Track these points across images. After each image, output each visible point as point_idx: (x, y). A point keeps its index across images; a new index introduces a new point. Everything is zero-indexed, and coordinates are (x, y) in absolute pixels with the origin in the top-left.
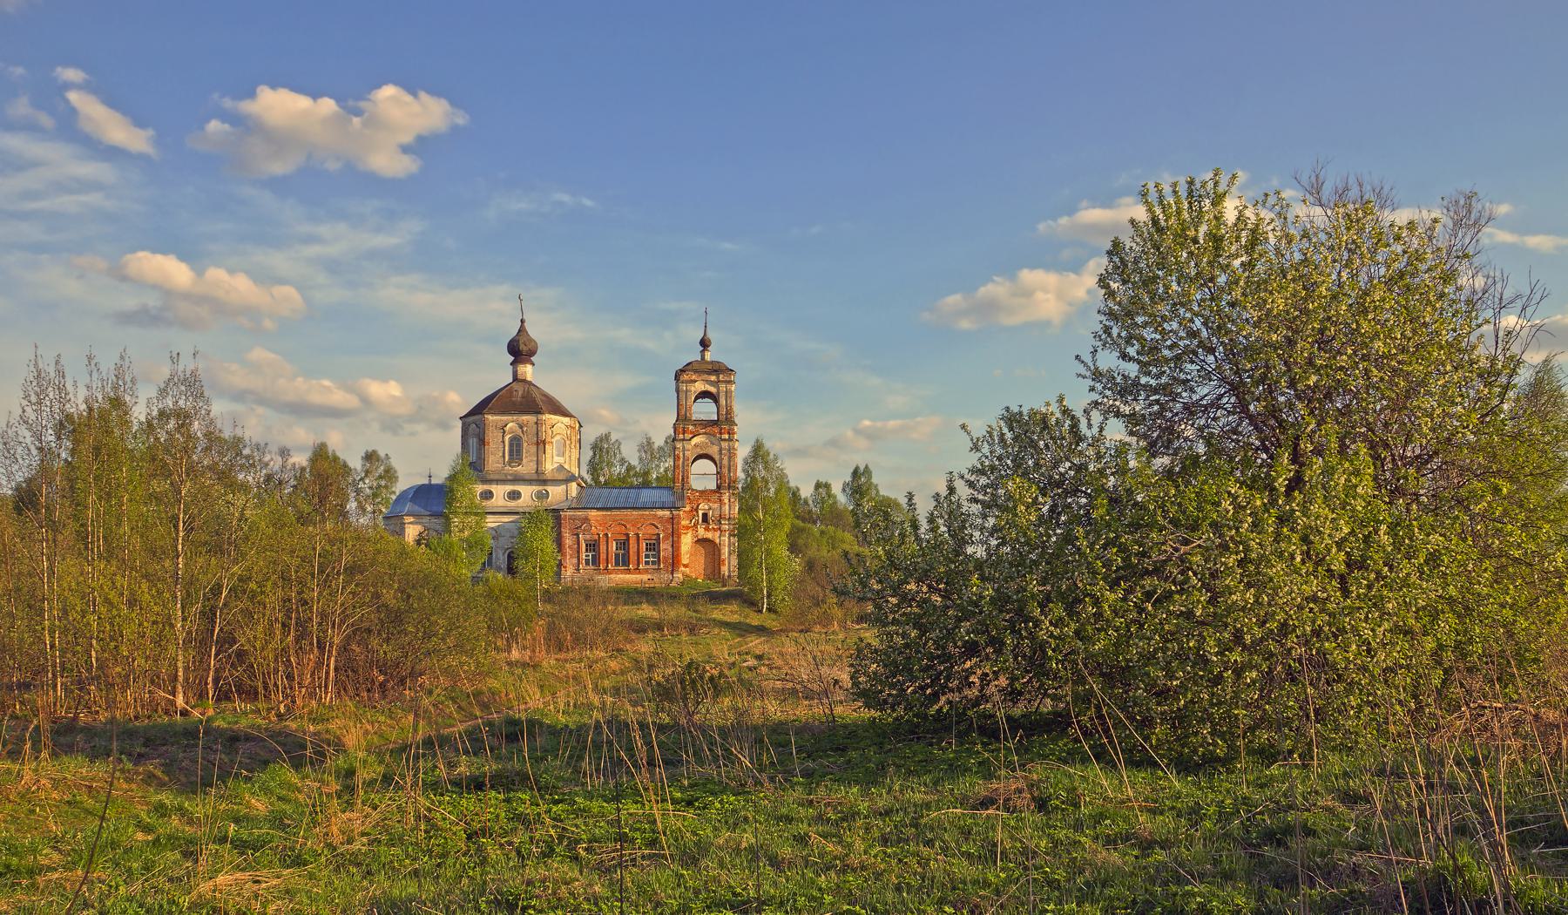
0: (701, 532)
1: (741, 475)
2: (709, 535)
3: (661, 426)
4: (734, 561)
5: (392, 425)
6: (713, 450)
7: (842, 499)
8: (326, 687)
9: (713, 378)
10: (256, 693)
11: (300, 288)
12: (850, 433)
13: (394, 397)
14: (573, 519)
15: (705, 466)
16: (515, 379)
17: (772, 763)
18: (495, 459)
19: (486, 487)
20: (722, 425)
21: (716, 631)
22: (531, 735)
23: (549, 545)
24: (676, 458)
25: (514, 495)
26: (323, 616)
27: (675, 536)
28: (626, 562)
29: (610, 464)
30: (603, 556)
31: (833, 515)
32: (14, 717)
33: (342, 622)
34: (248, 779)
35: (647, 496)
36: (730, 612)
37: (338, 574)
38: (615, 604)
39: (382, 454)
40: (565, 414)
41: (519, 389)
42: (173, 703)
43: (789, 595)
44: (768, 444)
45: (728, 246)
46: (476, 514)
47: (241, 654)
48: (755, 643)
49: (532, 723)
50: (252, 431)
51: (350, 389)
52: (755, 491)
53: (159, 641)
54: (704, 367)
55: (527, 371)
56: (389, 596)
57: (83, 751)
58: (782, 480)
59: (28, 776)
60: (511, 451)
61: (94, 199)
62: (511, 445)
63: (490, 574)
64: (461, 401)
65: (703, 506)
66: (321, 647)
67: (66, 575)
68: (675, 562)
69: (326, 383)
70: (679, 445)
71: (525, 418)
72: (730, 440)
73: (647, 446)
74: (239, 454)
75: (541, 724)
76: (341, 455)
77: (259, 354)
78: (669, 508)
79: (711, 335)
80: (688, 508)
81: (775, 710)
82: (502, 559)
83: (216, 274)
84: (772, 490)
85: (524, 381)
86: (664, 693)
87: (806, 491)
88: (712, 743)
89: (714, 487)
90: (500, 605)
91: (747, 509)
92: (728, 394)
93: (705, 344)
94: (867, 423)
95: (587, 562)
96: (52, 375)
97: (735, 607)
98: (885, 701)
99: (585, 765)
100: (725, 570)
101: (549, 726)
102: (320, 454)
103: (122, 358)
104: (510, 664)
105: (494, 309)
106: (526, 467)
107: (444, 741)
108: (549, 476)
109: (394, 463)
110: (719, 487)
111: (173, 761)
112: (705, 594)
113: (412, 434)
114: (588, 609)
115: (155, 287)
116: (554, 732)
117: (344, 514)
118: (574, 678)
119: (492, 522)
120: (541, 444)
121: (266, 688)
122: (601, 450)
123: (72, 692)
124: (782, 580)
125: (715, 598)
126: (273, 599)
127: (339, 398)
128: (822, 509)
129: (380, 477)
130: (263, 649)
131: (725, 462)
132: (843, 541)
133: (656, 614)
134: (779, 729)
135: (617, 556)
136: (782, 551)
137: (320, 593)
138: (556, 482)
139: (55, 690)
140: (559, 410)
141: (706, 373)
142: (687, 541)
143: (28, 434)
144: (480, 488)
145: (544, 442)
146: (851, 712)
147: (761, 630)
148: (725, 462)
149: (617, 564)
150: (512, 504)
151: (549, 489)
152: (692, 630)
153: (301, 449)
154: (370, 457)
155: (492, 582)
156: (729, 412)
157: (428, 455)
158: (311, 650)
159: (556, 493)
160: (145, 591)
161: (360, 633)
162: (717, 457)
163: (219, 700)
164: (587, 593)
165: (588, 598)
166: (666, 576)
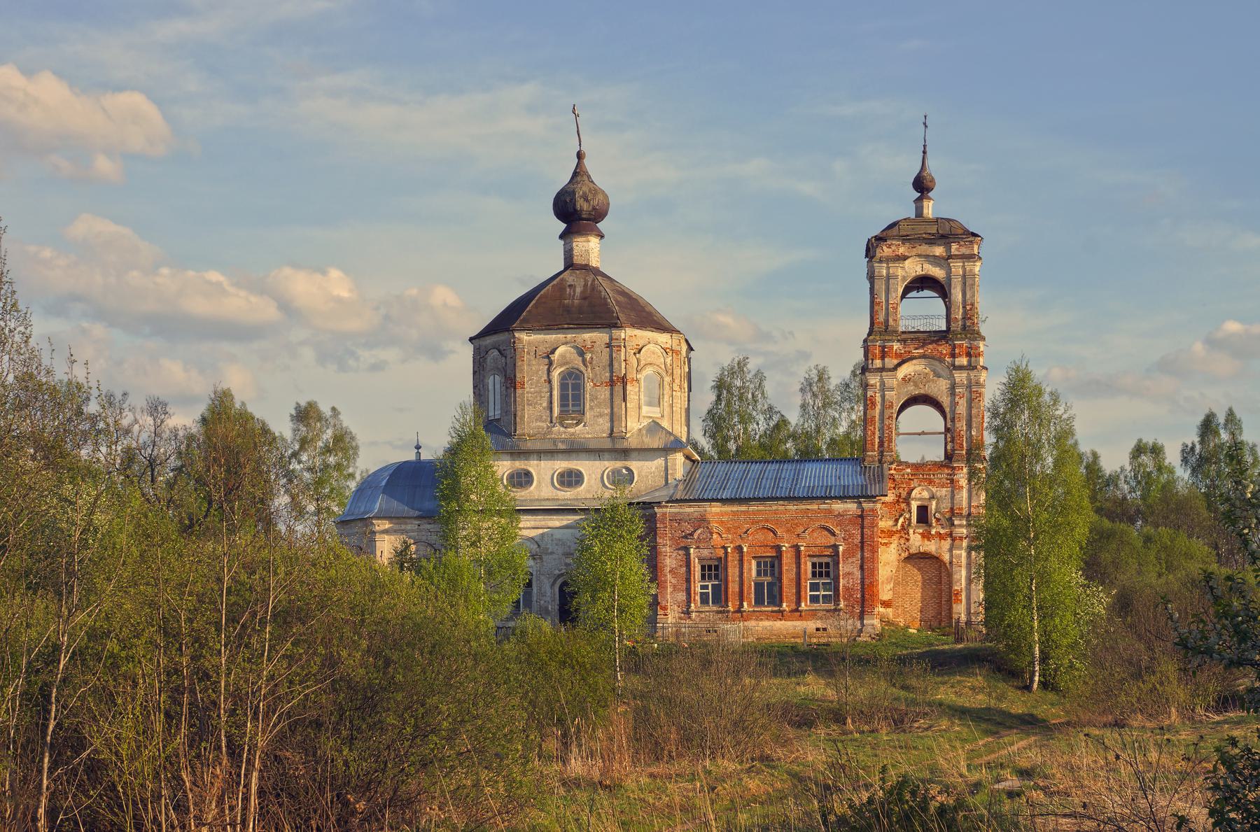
0: (916, 541)
2: (931, 547)
6: (939, 388)
9: (939, 251)
16: (569, 264)
18: (533, 416)
19: (519, 465)
25: (571, 479)
28: (776, 599)
30: (733, 587)
40: (661, 326)
54: (921, 230)
55: (590, 248)
60: (564, 398)
62: (563, 387)
65: (920, 494)
68: (865, 599)
70: (874, 380)
71: (587, 336)
72: (971, 367)
79: (933, 168)
85: (586, 268)
93: (922, 186)
95: (704, 599)
106: (593, 428)
110: (949, 457)
120: (618, 383)
135: (759, 586)
138: (645, 453)
140: (649, 319)
145: (624, 380)
148: (962, 409)
149: (759, 601)
150: (567, 495)
159: (646, 472)
166: (851, 624)
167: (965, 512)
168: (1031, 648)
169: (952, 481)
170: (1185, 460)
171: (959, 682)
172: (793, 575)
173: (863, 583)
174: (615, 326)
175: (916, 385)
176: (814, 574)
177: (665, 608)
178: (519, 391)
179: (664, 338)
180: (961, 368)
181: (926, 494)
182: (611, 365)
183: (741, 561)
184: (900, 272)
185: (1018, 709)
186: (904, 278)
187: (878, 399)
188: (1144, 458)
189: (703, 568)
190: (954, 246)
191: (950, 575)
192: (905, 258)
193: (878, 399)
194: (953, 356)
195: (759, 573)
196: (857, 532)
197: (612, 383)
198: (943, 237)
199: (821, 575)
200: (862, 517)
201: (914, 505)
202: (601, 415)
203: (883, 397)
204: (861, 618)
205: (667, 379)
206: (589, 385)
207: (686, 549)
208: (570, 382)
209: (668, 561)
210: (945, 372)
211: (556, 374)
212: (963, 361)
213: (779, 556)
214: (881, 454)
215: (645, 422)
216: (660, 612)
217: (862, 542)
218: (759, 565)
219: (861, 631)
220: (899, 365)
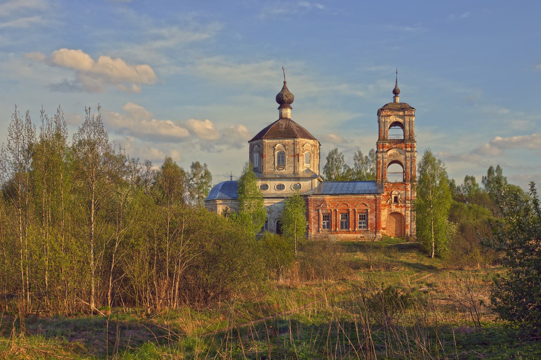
0: (394, 208)
1: (418, 175)
2: (398, 210)
3: (368, 143)
4: (414, 226)
5: (207, 146)
6: (401, 158)
7: (482, 186)
8: (174, 298)
9: (401, 113)
10: (135, 302)
11: (152, 67)
12: (487, 145)
13: (208, 130)
14: (315, 200)
15: (397, 168)
16: (281, 117)
17: (441, 351)
18: (269, 167)
19: (264, 182)
20: (407, 142)
21: (403, 269)
22: (294, 330)
23: (302, 217)
24: (378, 163)
25: (281, 187)
26: (172, 258)
27: (377, 211)
28: (347, 227)
29: (338, 168)
30: (333, 223)
31: (477, 198)
32: (6, 313)
33: (183, 262)
34: (132, 351)
35: (360, 186)
36: (412, 257)
37: (180, 234)
38: (341, 252)
39: (202, 164)
40: (311, 138)
41: (283, 123)
42: (89, 307)
43: (448, 247)
44: (434, 153)
45: (408, 29)
46: (257, 198)
47: (126, 280)
48: (428, 277)
49: (294, 323)
50: (129, 152)
51: (183, 126)
52: (426, 183)
53: (81, 271)
54: (396, 106)
55: (288, 112)
56: (209, 247)
57: (42, 333)
58: (443, 175)
59: (14, 346)
60: (279, 161)
61: (36, 19)
62: (279, 157)
63: (267, 233)
64: (248, 131)
66: (171, 275)
67: (30, 235)
68: (377, 227)
69: (169, 122)
70: (380, 155)
71: (287, 141)
72: (412, 151)
73: (359, 157)
74: (123, 165)
75: (299, 323)
76: (180, 165)
77: (130, 106)
78: (374, 194)
79: (400, 87)
80: (385, 194)
81: (439, 317)
82: (273, 225)
83: (104, 60)
84: (438, 182)
85: (286, 119)
86: (374, 305)
87: (459, 182)
88: (403, 337)
89: (400, 180)
90: (273, 252)
91: (422, 195)
92: (410, 123)
93: (396, 92)
94: (499, 138)
96: (24, 122)
97: (414, 254)
98: (514, 315)
99: (326, 348)
100: (408, 231)
101: (303, 325)
102: (168, 165)
103: (58, 111)
104: (280, 287)
105: (268, 76)
106: (288, 170)
107: (244, 332)
108: (301, 175)
109: (210, 169)
110: (404, 180)
111: (90, 339)
112: (396, 246)
113: (219, 151)
114: (325, 255)
115: (71, 69)
116: (305, 328)
117: (182, 201)
118: (317, 296)
119: (267, 203)
120: (296, 156)
121: (140, 299)
122: (332, 159)
123: (35, 300)
124: (444, 238)
125: (402, 248)
126: (143, 248)
127: (177, 131)
128: (469, 192)
129: (202, 177)
130: (138, 277)
131: (409, 165)
132: (483, 213)
133: (365, 258)
134: (445, 329)
135: (342, 223)
136: (444, 220)
137: (170, 245)
138: (305, 179)
139: (27, 300)
140: (306, 135)
141: (397, 111)
142: (384, 214)
143: (11, 156)
144: (259, 183)
145: (298, 155)
146: (490, 320)
147: (431, 268)
148: (409, 165)
149: (342, 228)
150: (280, 192)
151: (302, 183)
152: (388, 268)
153: (157, 161)
154: (196, 166)
155: (268, 239)
156: (411, 134)
157: (229, 164)
158: (166, 278)
159: (305, 185)
160: (73, 244)
161: (193, 268)
162: (403, 162)
163: (113, 306)
164: (324, 245)
165: (324, 248)
166: (372, 235)
167: (410, 199)
168: (431, 244)
169: (405, 189)
170: (483, 182)
171: (408, 255)
172: (353, 219)
173: (376, 222)
174: (296, 137)
175: (394, 157)
176: (360, 219)
177: (311, 230)
178: (264, 159)
179: (311, 141)
180: (408, 151)
181: (397, 193)
182: (294, 150)
183: (336, 214)
184: (388, 120)
185: (427, 264)
186: (390, 122)
187: (381, 161)
188: (468, 181)
189: (324, 216)
190: (406, 112)
191: (405, 219)
192: (390, 116)
193: (381, 161)
194: (406, 147)
195: (342, 219)
196: (374, 205)
197: (294, 156)
198: (403, 109)
199: (362, 219)
200: (376, 200)
201: (393, 196)
202: (291, 166)
203: (383, 161)
204: (376, 233)
205: (312, 155)
206: (287, 157)
207: (318, 210)
208: (281, 156)
209: (312, 214)
210: (403, 153)
211: (276, 153)
212: (409, 149)
213: (349, 213)
214: (382, 179)
215: (305, 169)
216: (309, 231)
217: (376, 208)
218: (342, 216)
219: (375, 238)
220: (388, 150)
